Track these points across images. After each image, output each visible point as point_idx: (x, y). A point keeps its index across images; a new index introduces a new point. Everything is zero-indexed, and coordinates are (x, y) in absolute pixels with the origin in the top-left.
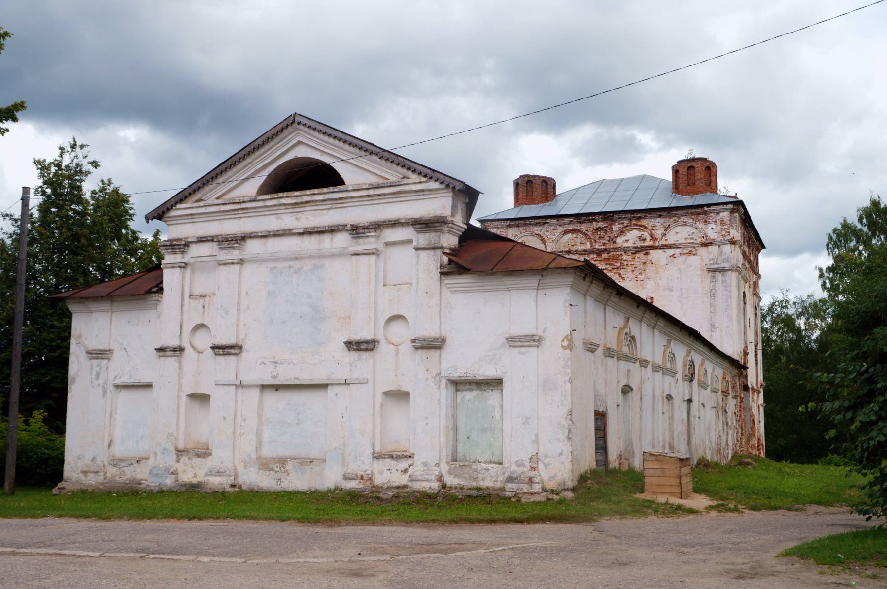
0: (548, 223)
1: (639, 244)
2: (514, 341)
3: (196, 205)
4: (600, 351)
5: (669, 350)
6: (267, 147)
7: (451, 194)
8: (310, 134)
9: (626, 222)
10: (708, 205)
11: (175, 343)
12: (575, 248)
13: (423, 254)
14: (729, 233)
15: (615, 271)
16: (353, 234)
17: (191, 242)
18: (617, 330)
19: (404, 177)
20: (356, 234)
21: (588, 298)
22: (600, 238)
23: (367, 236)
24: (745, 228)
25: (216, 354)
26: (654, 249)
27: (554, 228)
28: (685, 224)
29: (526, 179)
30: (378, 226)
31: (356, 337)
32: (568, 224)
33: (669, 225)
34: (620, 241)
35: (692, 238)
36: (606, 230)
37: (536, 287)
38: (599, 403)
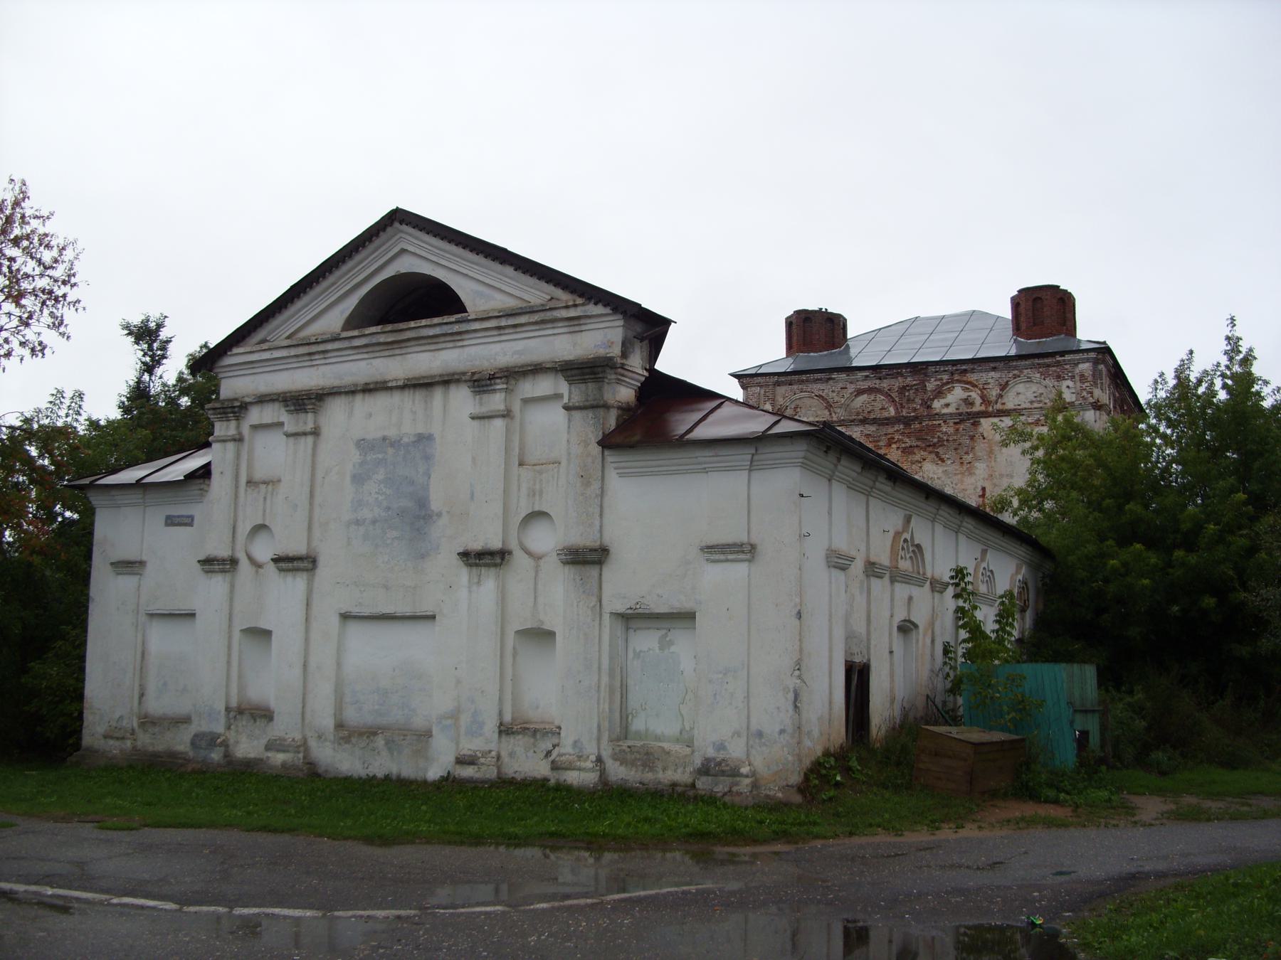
0: (834, 379)
1: (964, 409)
2: (719, 551)
3: (258, 348)
4: (858, 567)
5: (984, 565)
6: (358, 258)
7: (621, 323)
8: (417, 238)
9: (945, 377)
10: (1062, 354)
11: (224, 552)
12: (872, 416)
13: (577, 415)
14: (1091, 393)
15: (931, 449)
16: (474, 387)
17: (251, 403)
18: (891, 534)
19: (552, 298)
20: (479, 387)
21: (835, 484)
22: (908, 400)
23: (494, 390)
24: (1117, 386)
25: (207, 572)
26: (986, 417)
27: (843, 386)
28: (1030, 380)
29: (803, 316)
30: (513, 374)
31: (477, 546)
32: (863, 380)
33: (1007, 382)
34: (937, 404)
35: (1040, 401)
36: (917, 390)
37: (748, 467)
38: (855, 650)
